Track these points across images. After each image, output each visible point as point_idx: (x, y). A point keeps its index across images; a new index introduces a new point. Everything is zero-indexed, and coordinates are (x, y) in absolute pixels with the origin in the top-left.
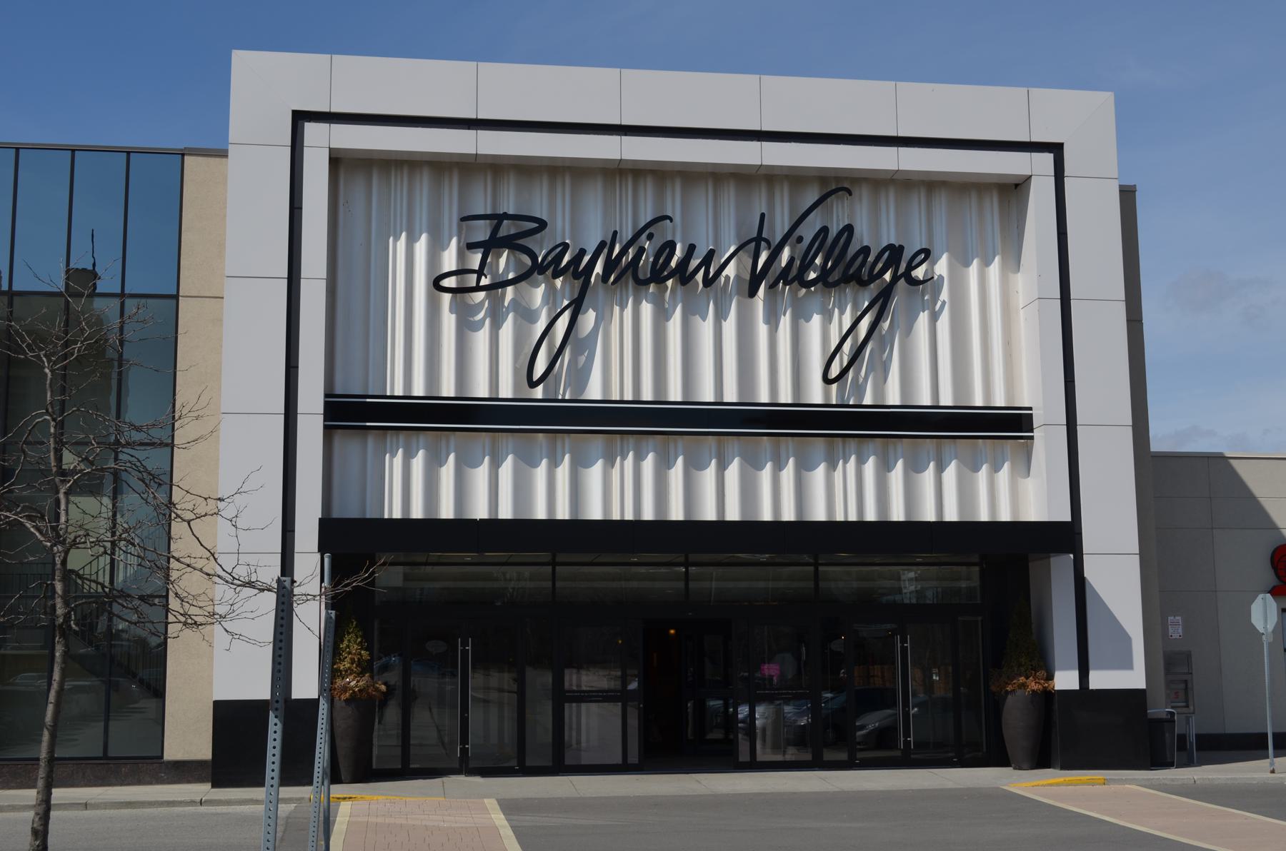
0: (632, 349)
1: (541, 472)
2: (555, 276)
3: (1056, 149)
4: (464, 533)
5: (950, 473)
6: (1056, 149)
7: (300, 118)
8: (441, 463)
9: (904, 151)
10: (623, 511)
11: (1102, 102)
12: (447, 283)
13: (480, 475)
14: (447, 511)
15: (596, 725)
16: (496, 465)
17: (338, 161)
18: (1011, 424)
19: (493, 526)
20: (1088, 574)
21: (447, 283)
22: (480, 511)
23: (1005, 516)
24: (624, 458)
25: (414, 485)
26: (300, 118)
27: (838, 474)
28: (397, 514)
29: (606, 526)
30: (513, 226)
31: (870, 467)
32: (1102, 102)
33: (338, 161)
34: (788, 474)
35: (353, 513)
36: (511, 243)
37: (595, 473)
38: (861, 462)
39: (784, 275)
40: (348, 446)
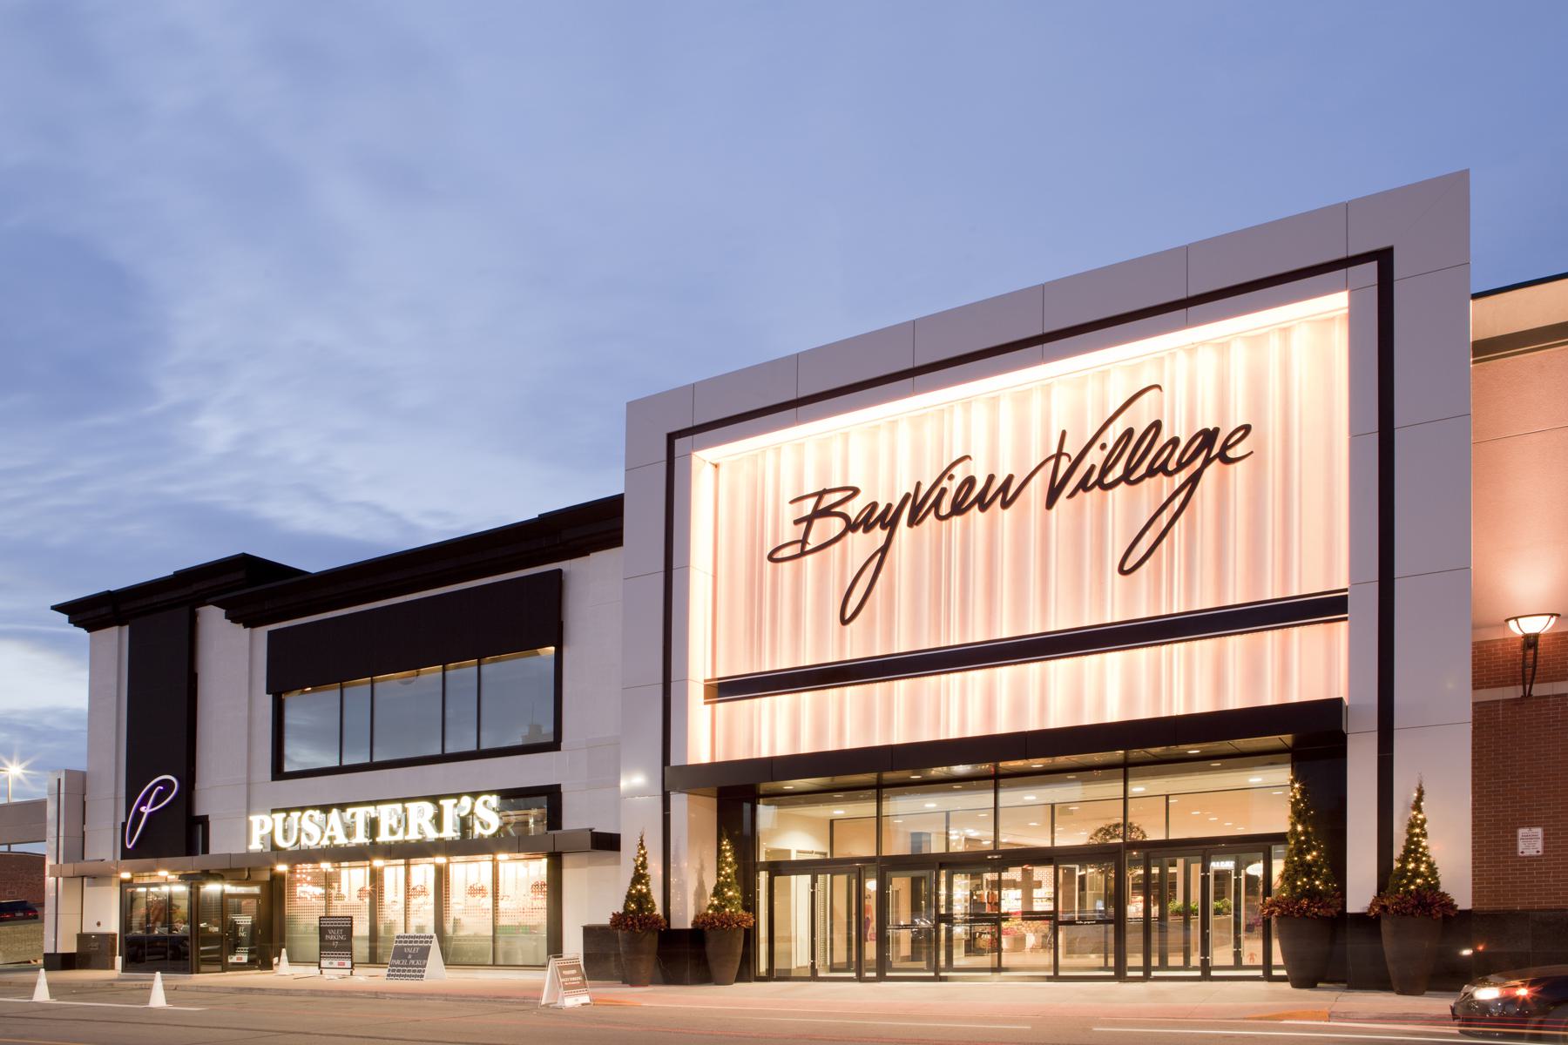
23: (720, 758)
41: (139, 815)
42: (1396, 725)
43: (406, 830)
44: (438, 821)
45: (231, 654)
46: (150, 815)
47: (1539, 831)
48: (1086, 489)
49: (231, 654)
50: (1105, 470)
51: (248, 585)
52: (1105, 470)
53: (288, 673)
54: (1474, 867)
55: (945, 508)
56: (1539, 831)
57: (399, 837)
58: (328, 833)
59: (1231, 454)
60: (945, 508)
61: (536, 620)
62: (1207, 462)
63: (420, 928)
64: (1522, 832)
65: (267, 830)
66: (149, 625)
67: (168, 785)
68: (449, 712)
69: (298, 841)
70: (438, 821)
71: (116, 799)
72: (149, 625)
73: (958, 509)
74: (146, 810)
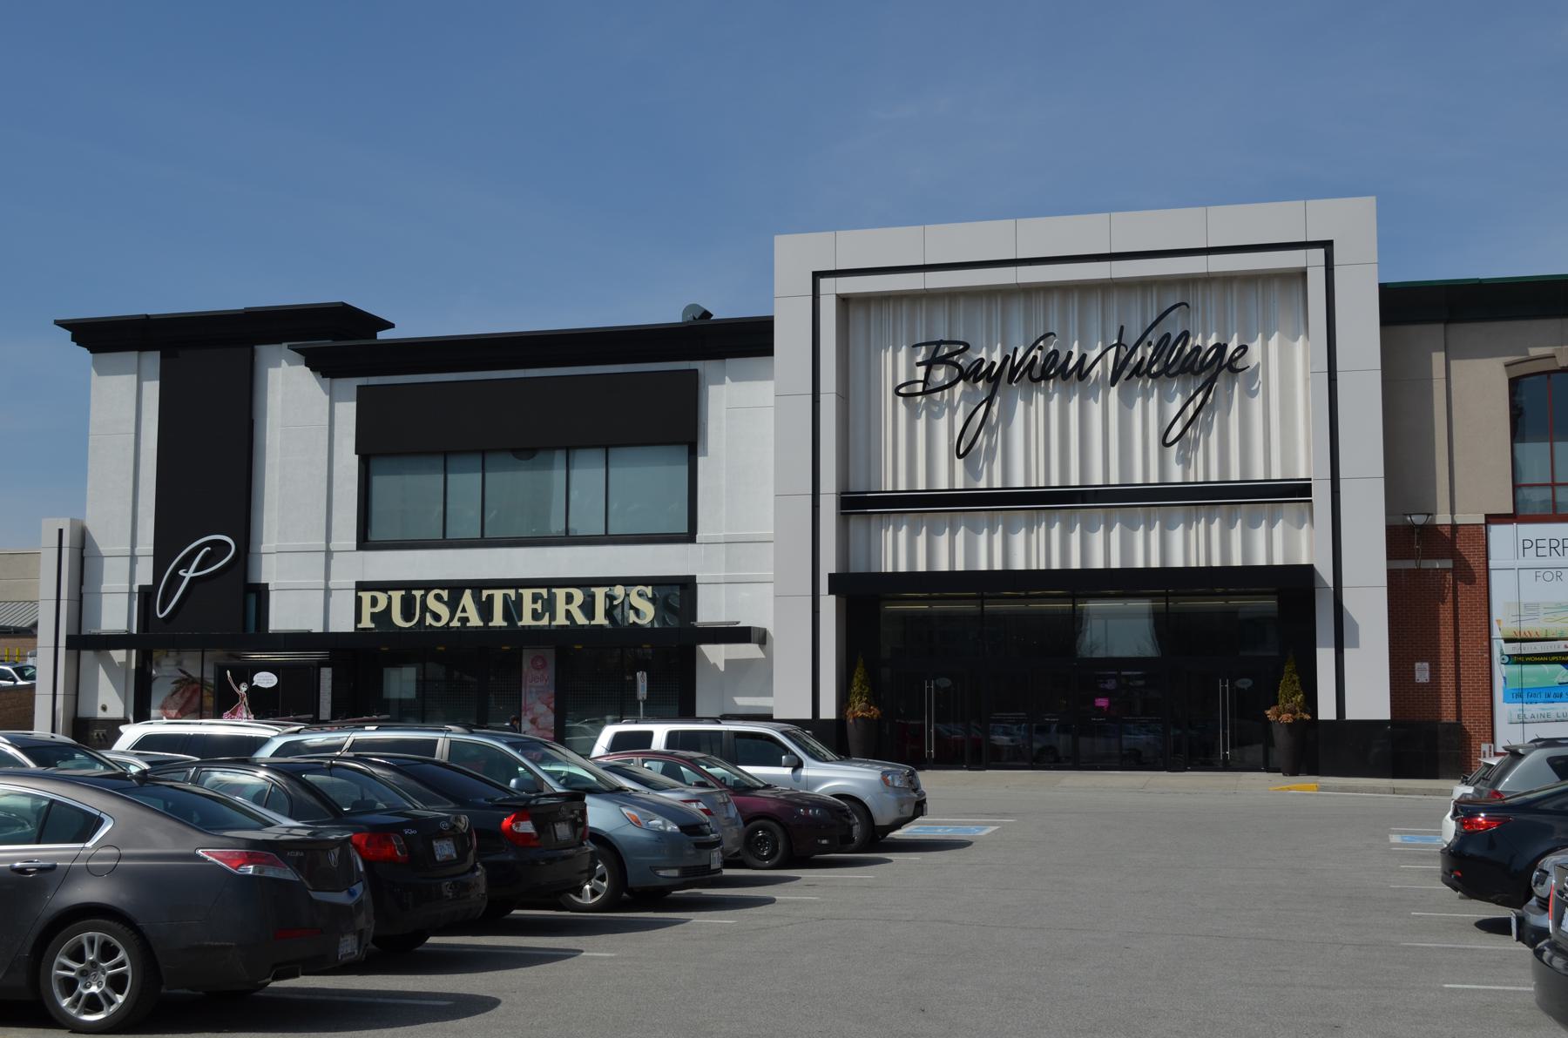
0: (1037, 440)
1: (983, 539)
2: (976, 380)
3: (817, 276)
4: (952, 580)
5: (1278, 530)
6: (817, 276)
7: (1327, 245)
8: (919, 533)
9: (1115, 264)
10: (1197, 560)
11: (1365, 207)
12: (902, 390)
13: (1098, 538)
14: (1237, 561)
15: (174, 712)
16: (1108, 529)
17: (844, 301)
18: (1299, 491)
19: (952, 576)
20: (1347, 603)
21: (902, 390)
22: (943, 566)
23: (1278, 561)
24: (1198, 522)
25: (900, 549)
26: (1327, 245)
27: (1193, 533)
28: (890, 570)
29: (1186, 572)
30: (988, 345)
31: (1216, 527)
32: (1365, 207)
33: (844, 301)
34: (1155, 534)
35: (862, 569)
36: (944, 360)
37: (1177, 535)
38: (1209, 522)
39: (1137, 371)
40: (856, 524)
41: (175, 579)
42: (1385, 591)
43: (553, 617)
44: (588, 608)
45: (303, 422)
46: (192, 579)
47: (1426, 665)
48: (1139, 376)
49: (303, 422)
50: (1151, 364)
51: (336, 339)
52: (1151, 364)
53: (378, 445)
54: (419, 1023)
55: (1036, 373)
56: (1426, 665)
57: (545, 621)
58: (459, 614)
59: (1239, 365)
60: (1036, 373)
61: (677, 428)
62: (1220, 368)
63: (1145, 627)
64: (1418, 665)
65: (382, 606)
66: (1487, 516)
67: (219, 549)
68: (613, 507)
69: (422, 618)
70: (588, 608)
71: (133, 558)
72: (1487, 516)
73: (1045, 376)
74: (188, 575)
